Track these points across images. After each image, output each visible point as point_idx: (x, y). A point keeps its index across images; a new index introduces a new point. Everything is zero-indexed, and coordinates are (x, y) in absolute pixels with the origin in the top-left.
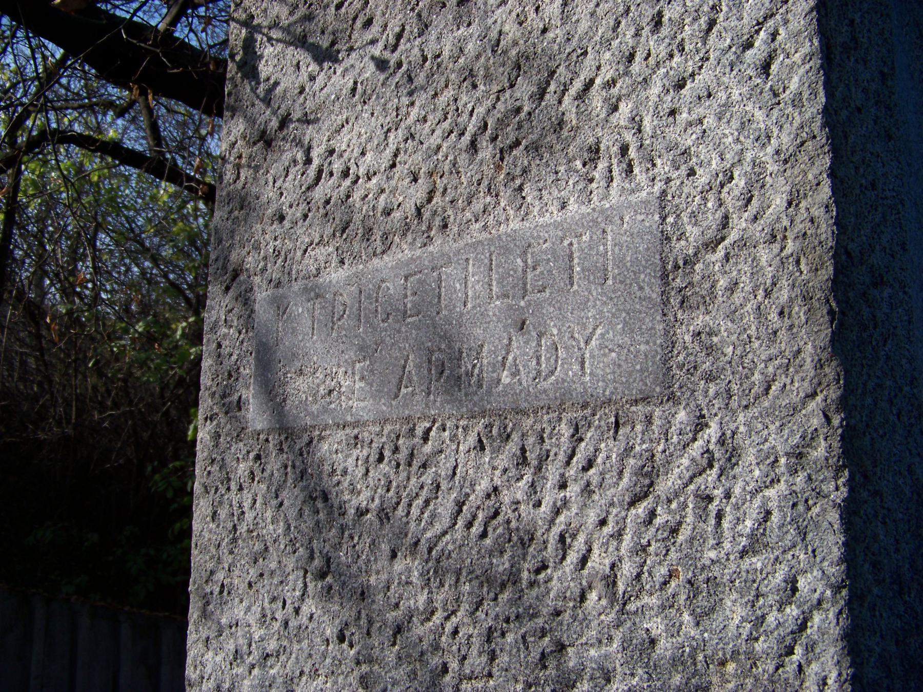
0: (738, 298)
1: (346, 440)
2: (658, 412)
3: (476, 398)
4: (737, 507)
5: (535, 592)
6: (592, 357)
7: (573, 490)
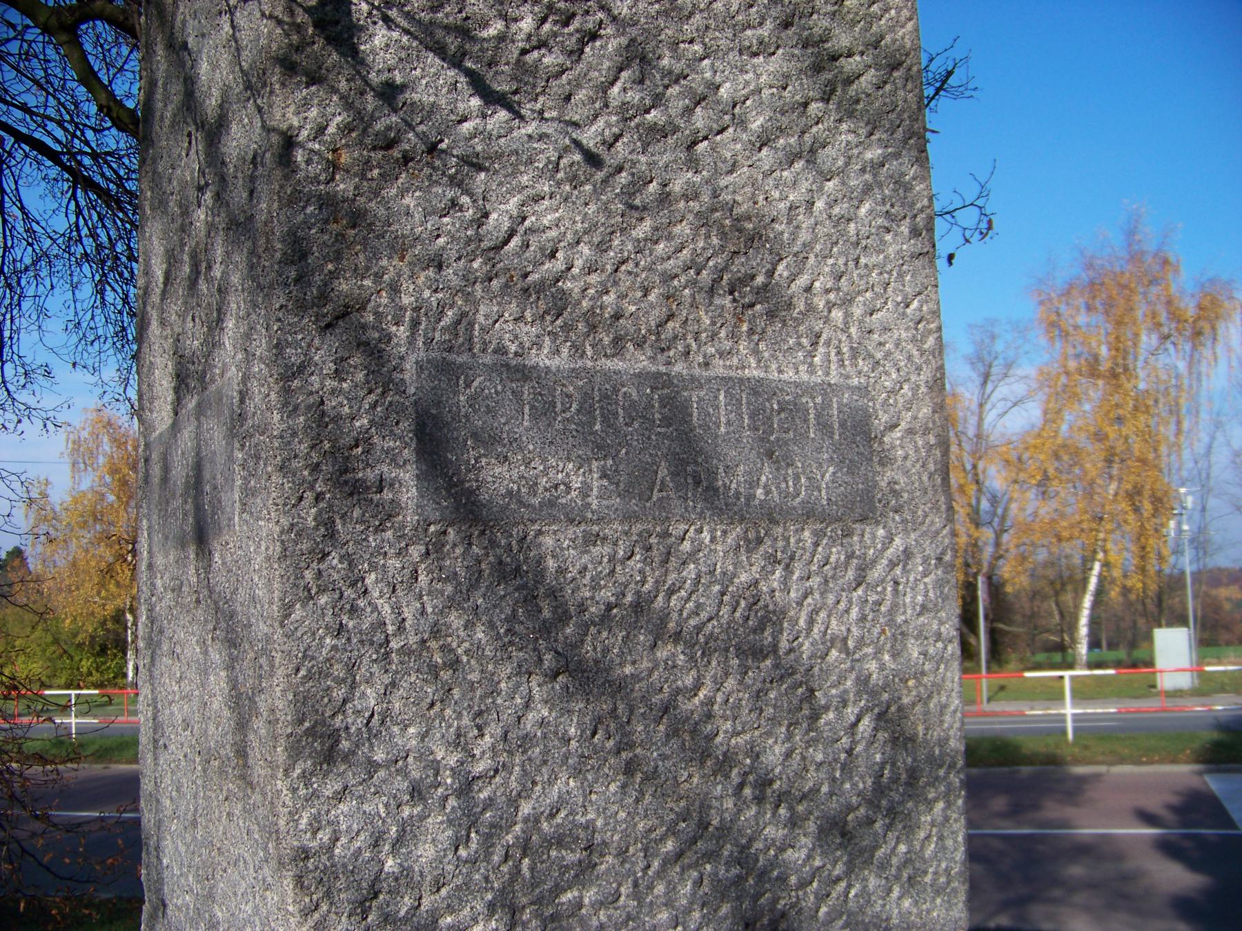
0: (908, 463)
1: (584, 537)
2: (868, 529)
3: (735, 508)
4: (912, 589)
5: (792, 656)
6: (828, 487)
7: (815, 581)
